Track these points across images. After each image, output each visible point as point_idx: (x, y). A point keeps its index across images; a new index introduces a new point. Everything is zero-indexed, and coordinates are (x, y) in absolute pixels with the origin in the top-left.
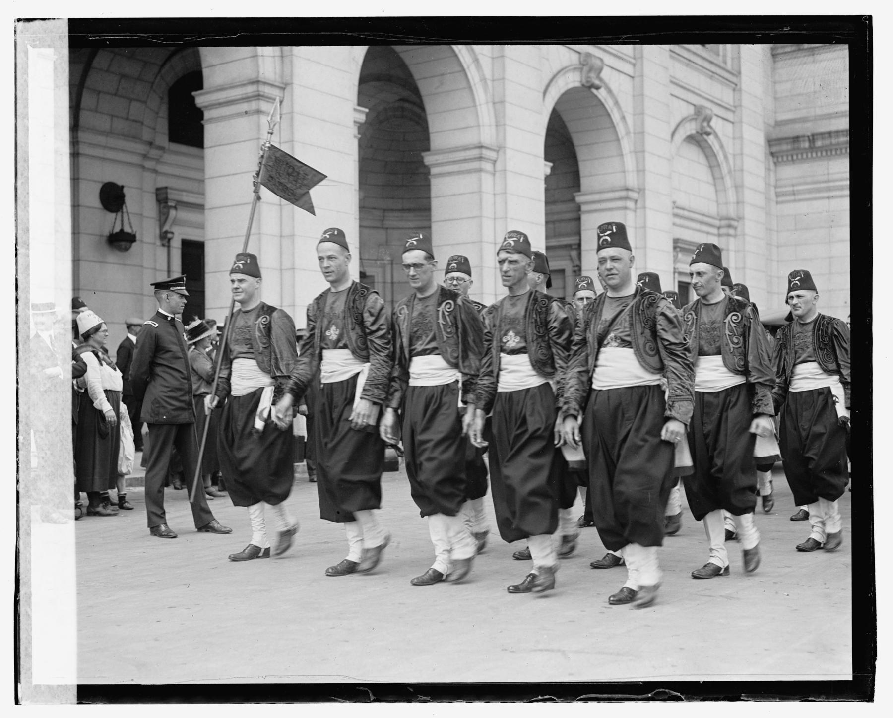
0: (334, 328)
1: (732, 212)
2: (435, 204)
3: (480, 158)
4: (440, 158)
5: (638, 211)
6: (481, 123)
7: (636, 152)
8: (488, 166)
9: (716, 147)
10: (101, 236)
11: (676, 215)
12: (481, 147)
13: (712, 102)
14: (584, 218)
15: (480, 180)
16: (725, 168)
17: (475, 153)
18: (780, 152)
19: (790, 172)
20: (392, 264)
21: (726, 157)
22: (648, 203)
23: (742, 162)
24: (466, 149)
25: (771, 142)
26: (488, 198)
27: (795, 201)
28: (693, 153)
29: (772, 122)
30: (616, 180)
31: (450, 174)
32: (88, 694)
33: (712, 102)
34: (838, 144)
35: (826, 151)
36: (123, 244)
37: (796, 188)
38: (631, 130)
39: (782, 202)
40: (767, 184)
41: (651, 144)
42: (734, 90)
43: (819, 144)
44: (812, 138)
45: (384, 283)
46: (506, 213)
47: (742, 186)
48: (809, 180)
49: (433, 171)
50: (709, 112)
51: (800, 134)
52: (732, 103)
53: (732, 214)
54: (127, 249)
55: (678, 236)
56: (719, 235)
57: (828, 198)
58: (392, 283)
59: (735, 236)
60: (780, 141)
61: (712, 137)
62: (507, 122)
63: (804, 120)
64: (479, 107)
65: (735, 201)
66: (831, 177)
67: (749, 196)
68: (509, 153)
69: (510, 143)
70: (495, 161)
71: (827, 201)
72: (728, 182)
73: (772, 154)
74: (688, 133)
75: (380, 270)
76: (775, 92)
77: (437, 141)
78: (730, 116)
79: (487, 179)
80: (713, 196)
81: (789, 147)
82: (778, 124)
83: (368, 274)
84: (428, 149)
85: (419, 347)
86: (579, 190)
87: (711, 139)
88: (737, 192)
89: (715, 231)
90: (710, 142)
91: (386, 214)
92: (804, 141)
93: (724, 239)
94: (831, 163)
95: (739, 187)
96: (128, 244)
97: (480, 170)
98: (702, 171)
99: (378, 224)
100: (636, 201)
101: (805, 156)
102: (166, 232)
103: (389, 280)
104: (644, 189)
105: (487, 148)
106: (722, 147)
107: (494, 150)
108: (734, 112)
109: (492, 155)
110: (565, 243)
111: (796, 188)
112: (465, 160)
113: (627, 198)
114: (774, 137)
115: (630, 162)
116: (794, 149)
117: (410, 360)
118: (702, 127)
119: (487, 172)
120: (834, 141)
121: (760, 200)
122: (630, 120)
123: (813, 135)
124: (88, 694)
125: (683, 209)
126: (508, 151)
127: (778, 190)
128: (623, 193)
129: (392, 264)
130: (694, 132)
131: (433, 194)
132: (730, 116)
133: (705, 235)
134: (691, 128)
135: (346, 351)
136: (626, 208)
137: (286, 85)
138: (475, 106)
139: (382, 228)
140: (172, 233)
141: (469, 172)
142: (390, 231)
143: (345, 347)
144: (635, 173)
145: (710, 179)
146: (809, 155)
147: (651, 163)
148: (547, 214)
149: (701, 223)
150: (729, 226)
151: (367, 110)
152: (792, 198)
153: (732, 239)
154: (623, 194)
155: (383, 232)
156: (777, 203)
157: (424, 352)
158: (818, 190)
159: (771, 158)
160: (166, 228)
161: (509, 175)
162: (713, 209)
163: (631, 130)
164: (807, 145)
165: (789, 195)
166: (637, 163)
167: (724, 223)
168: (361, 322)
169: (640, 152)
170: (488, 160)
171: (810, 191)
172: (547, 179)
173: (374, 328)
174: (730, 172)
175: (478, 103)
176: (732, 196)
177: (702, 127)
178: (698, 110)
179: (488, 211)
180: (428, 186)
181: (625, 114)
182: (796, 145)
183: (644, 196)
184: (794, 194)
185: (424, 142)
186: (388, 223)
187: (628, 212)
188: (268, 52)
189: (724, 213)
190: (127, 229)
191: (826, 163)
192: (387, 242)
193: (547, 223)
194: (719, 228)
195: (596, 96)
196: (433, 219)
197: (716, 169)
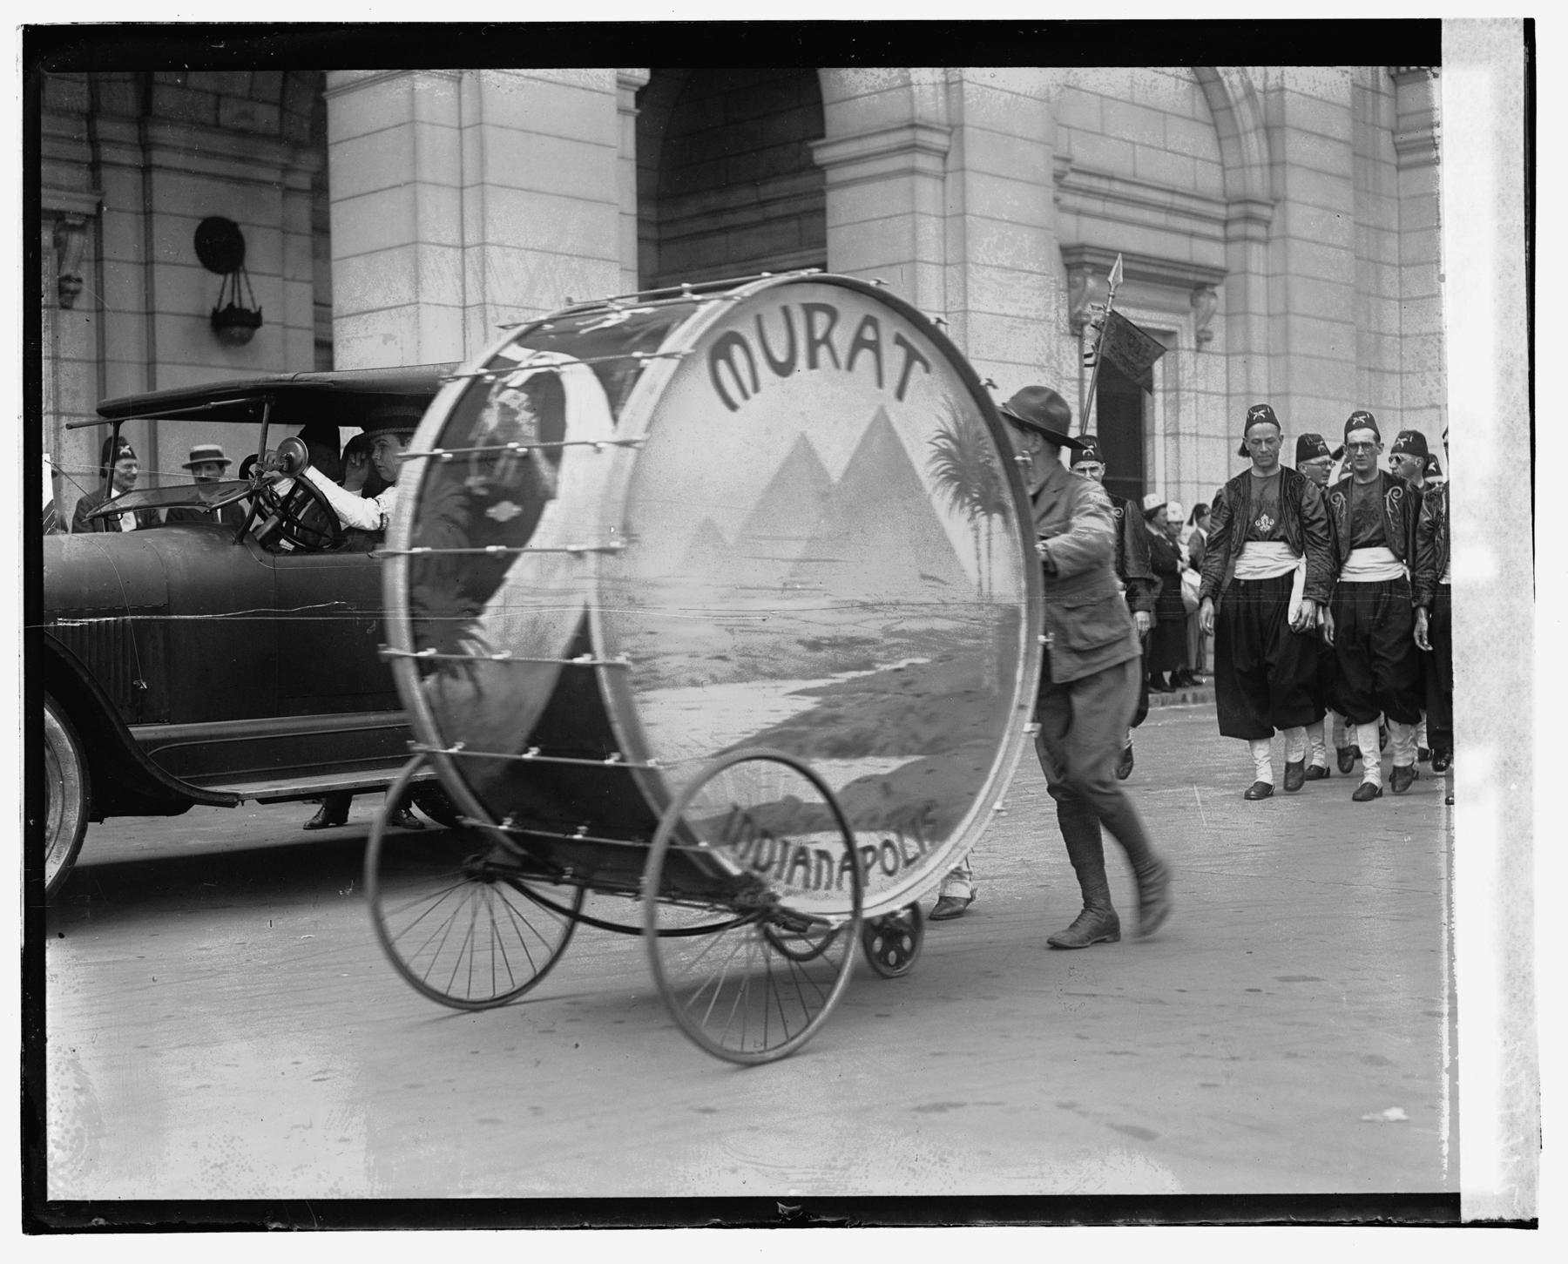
0: (1265, 517)
1: (1257, 182)
5: (950, 177)
10: (202, 317)
22: (973, 158)
36: (237, 331)
39: (1410, 166)
47: (1282, 126)
54: (244, 340)
55: (1071, 240)
56: (1227, 240)
59: (1266, 242)
85: (1362, 537)
86: (822, 136)
89: (1218, 231)
93: (1236, 248)
96: (245, 331)
102: (68, 278)
104: (962, 125)
109: (939, 141)
117: (1349, 553)
121: (1335, 158)
125: (1111, 178)
127: (1398, 138)
128: (905, 136)
131: (830, 223)
133: (1184, 240)
135: (1282, 544)
136: (913, 171)
137: (1277, 200)
140: (79, 281)
143: (1282, 539)
145: (1201, 110)
149: (1170, 210)
150: (1249, 218)
153: (1256, 250)
156: (1399, 168)
157: (1368, 544)
160: (68, 270)
162: (1211, 180)
167: (1235, 210)
168: (1298, 510)
170: (926, 149)
173: (1315, 517)
176: (1255, 147)
187: (919, 180)
188: (926, 78)
189: (1235, 187)
190: (247, 304)
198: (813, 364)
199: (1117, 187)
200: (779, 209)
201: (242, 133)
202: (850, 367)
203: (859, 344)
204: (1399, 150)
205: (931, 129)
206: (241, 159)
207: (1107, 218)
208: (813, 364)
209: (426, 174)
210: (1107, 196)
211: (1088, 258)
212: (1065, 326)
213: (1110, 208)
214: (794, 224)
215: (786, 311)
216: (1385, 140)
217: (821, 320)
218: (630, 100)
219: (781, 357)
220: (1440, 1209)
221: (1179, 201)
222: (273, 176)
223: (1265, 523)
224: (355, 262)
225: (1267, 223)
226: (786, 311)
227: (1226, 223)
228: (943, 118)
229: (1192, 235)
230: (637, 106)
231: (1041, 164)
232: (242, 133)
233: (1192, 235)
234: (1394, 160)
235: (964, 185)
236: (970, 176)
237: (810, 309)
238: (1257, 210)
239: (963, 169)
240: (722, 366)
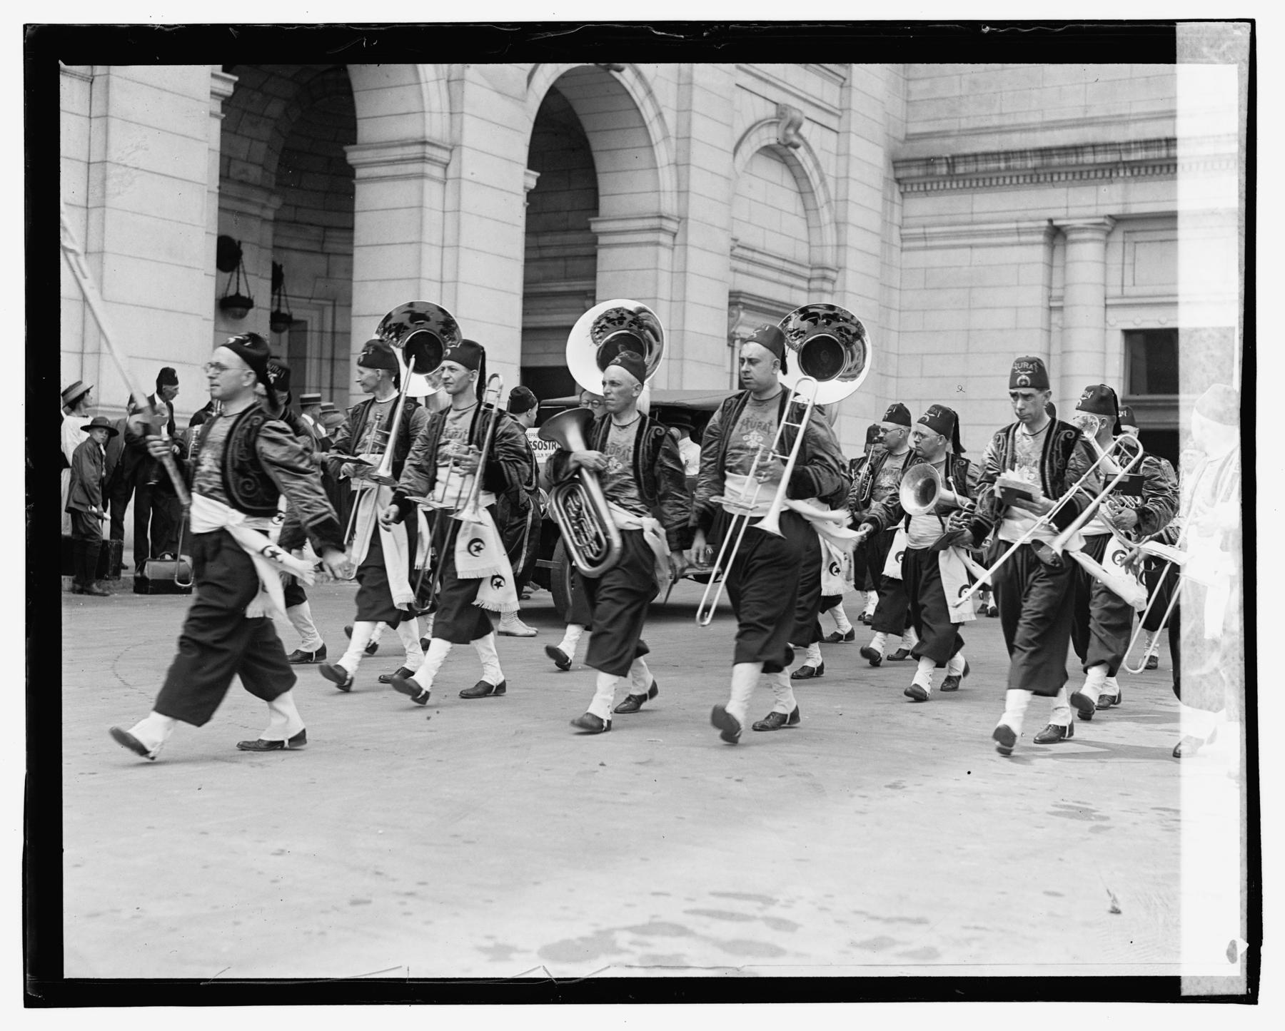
1: (829, 258)
2: (359, 220)
3: (423, 159)
4: (369, 155)
5: (677, 248)
6: (427, 109)
7: (676, 164)
8: (437, 171)
9: (808, 165)
11: (734, 257)
12: (424, 143)
13: (805, 100)
14: (602, 253)
15: (421, 190)
16: (821, 197)
17: (415, 150)
18: (908, 178)
19: (923, 207)
20: (334, 306)
21: (822, 180)
22: (692, 239)
23: (847, 190)
24: (404, 144)
25: (897, 163)
26: (432, 217)
27: (926, 248)
28: (773, 170)
29: (902, 137)
30: (646, 203)
31: (381, 179)
32: (1151, 42)
33: (805, 100)
34: (986, 172)
35: (971, 181)
36: (239, 310)
37: (927, 230)
38: (672, 132)
39: (909, 249)
40: (886, 222)
41: (699, 154)
42: (841, 86)
43: (960, 169)
44: (952, 161)
45: (322, 332)
46: (458, 240)
48: (946, 219)
49: (360, 173)
50: (796, 115)
51: (937, 153)
52: (836, 104)
53: (830, 260)
54: (242, 316)
55: (737, 288)
56: (809, 290)
57: (971, 246)
58: (333, 333)
60: (908, 162)
61: (801, 150)
62: (466, 110)
63: (944, 134)
64: (424, 86)
65: (835, 242)
66: (976, 217)
67: (854, 237)
68: (466, 153)
69: (469, 138)
70: (447, 165)
71: (968, 251)
72: (826, 216)
73: (898, 181)
74: (765, 143)
75: (316, 314)
76: (909, 93)
77: (366, 131)
78: (833, 122)
79: (432, 192)
80: (803, 235)
81: (921, 172)
82: (910, 138)
83: (295, 317)
84: (353, 140)
86: (597, 215)
87: (801, 153)
88: (838, 231)
89: (804, 284)
90: (800, 159)
91: (328, 233)
92: (941, 164)
94: (977, 197)
95: (839, 225)
97: (422, 176)
98: (787, 198)
99: (316, 247)
100: (675, 235)
101: (941, 186)
103: (328, 328)
105: (433, 145)
106: (817, 165)
107: (446, 149)
108: (840, 117)
109: (672, 226)
110: (578, 288)
111: (927, 230)
112: (403, 161)
113: (660, 229)
114: (903, 156)
115: (667, 178)
116: (927, 175)
118: (786, 135)
119: (433, 179)
120: (981, 167)
121: (873, 244)
122: (670, 117)
123: (953, 157)
124: (1151, 42)
125: (754, 250)
126: (465, 150)
128: (655, 223)
129: (334, 306)
130: (773, 142)
131: (358, 207)
132: (833, 122)
133: (787, 289)
134: (770, 136)
136: (658, 244)
138: (419, 83)
139: (322, 253)
141: (407, 177)
142: (332, 258)
144: (675, 194)
145: (800, 209)
146: (948, 185)
147: (698, 182)
148: (527, 248)
149: (782, 271)
150: (824, 278)
151: (236, 79)
152: (922, 244)
154: (655, 223)
155: (322, 259)
156: (902, 250)
158: (958, 235)
159: (896, 186)
161: (465, 184)
162: (802, 254)
163: (672, 132)
164: (944, 170)
165: (920, 239)
166: (678, 181)
167: (817, 273)
169: (682, 165)
170: (434, 161)
171: (947, 236)
172: (531, 195)
174: (828, 202)
175: (423, 79)
176: (830, 236)
177: (786, 135)
178: (782, 110)
179: (432, 235)
180: (350, 194)
181: (663, 110)
182: (930, 170)
183: (686, 230)
184: (925, 239)
185: (348, 132)
186: (330, 247)
187: (661, 249)
189: (817, 259)
190: (244, 293)
191: (970, 196)
192: (328, 273)
193: (527, 260)
194: (809, 280)
195: (618, 81)
196: (356, 242)
197: (808, 197)
199: (757, 257)
200: (552, 252)
201: (241, 182)
204: (903, 239)
205: (439, 147)
206: (241, 200)
207: (748, 274)
209: (426, 238)
210: (750, 261)
211: (742, 300)
212: (726, 342)
213: (751, 268)
214: (561, 263)
216: (896, 233)
218: (217, 107)
220: (1164, 989)
221: (787, 266)
222: (256, 211)
224: (371, 286)
225: (834, 282)
228: (675, 213)
229: (792, 286)
230: (223, 111)
231: (725, 244)
232: (241, 182)
233: (792, 286)
234: (899, 244)
235: (686, 254)
236: (689, 248)
238: (829, 274)
239: (686, 245)
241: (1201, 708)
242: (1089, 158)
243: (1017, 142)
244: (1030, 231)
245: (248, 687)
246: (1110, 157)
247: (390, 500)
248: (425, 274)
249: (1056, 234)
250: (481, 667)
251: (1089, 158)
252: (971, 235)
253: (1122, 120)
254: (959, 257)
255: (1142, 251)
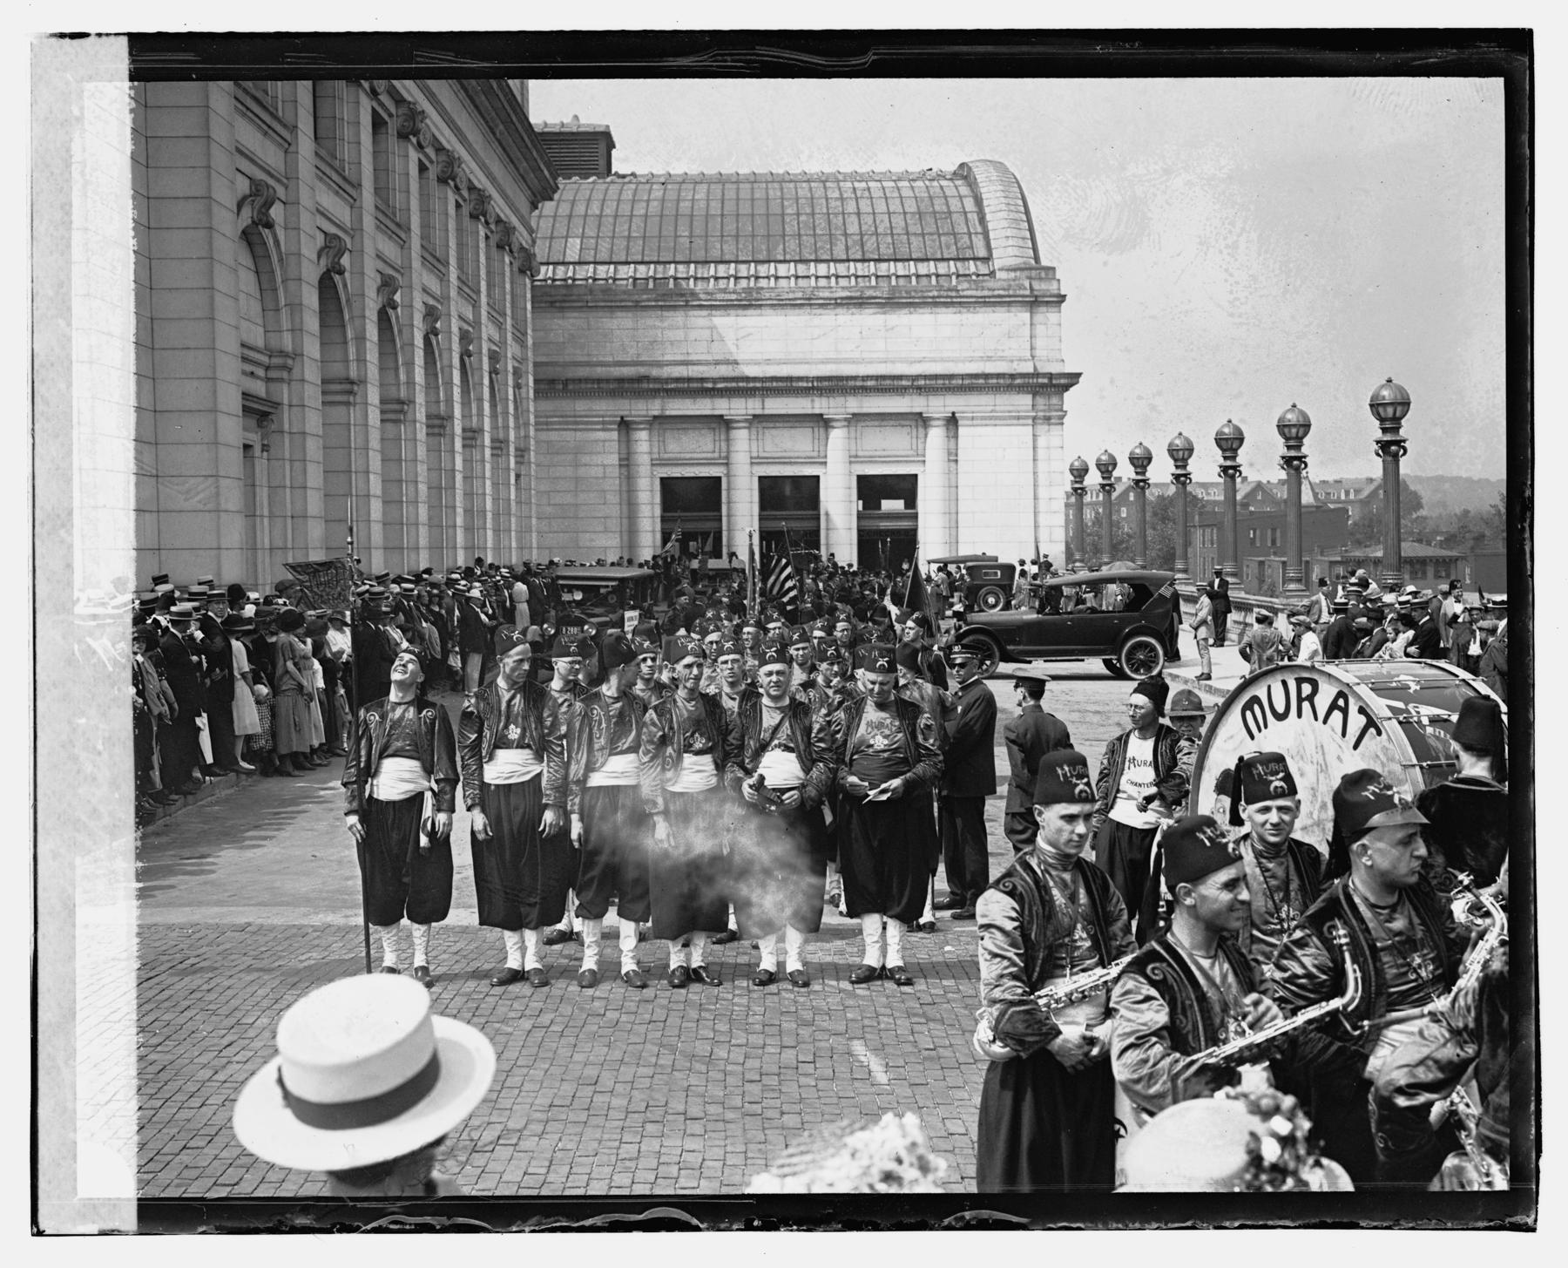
43: (570, 387)
44: (566, 382)
59: (289, 382)
128: (348, 387)
135: (527, 751)
143: (529, 746)
158: (567, 423)
167: (276, 361)
189: (274, 343)
198: (1300, 715)
202: (1325, 722)
203: (1333, 706)
208: (1300, 715)
215: (1284, 683)
217: (1307, 689)
219: (1280, 709)
223: (514, 733)
226: (1284, 683)
227: (267, 368)
237: (1299, 681)
240: (1248, 714)
241: (74, 937)
242: (645, 385)
243: (600, 372)
244: (611, 423)
245: (1311, 848)
246: (657, 386)
247: (345, 806)
248: (373, 544)
249: (625, 426)
250: (862, 953)
251: (645, 385)
252: (576, 423)
253: (659, 364)
254: (569, 435)
255: (668, 434)
